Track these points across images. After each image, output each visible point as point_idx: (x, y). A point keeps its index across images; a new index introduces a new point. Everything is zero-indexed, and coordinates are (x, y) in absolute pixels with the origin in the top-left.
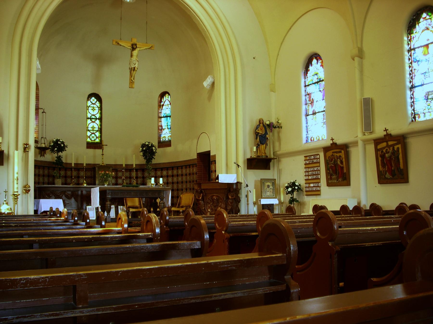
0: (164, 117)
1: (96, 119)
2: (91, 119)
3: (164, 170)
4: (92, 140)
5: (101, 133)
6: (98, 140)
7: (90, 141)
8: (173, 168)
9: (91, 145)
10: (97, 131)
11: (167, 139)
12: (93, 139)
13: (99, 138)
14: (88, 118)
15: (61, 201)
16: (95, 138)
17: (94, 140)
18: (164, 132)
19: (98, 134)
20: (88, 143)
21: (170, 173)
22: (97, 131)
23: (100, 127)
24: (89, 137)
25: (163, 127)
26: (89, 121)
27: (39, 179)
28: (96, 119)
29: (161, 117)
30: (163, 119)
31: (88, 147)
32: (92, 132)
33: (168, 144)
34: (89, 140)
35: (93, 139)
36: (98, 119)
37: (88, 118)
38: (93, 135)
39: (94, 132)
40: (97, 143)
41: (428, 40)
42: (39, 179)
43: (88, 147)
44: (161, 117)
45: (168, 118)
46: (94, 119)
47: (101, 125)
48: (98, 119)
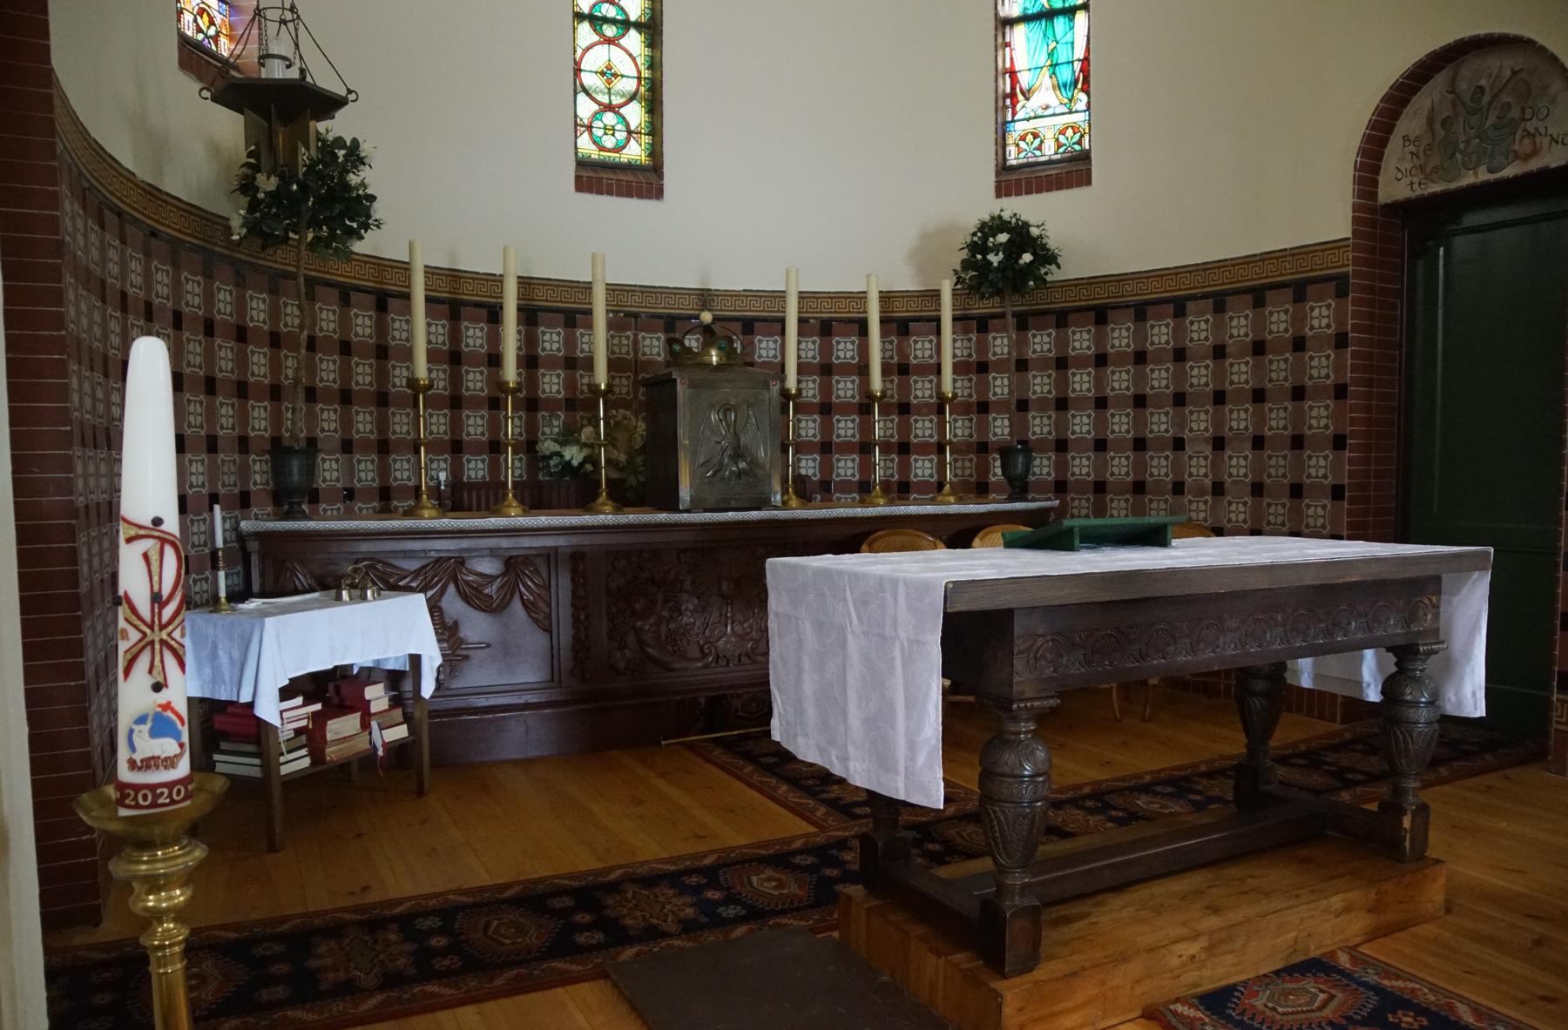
0: (1026, 19)
1: (626, 24)
2: (596, 21)
3: (1160, 317)
4: (602, 148)
5: (654, 106)
6: (636, 152)
7: (595, 154)
8: (1258, 297)
9: (596, 177)
10: (633, 97)
11: (1049, 150)
12: (609, 142)
13: (646, 139)
14: (580, 17)
15: (417, 603)
16: (621, 136)
17: (618, 149)
18: (1025, 108)
19: (636, 114)
20: (583, 164)
21: (1081, 341)
22: (633, 97)
23: (646, 74)
24: (590, 128)
25: (1025, 79)
26: (585, 33)
27: (211, 415)
28: (626, 24)
29: (1010, 22)
30: (1019, 34)
31: (583, 185)
32: (605, 99)
33: (1073, 170)
34: (585, 145)
35: (609, 142)
36: (638, 26)
37: (580, 17)
38: (609, 118)
39: (616, 100)
40: (629, 167)
41: (1047, 107)
42: (211, 415)
43: (583, 185)
44: (1010, 22)
45: (1060, 22)
46: (613, 21)
47: (654, 64)
48: (638, 26)
